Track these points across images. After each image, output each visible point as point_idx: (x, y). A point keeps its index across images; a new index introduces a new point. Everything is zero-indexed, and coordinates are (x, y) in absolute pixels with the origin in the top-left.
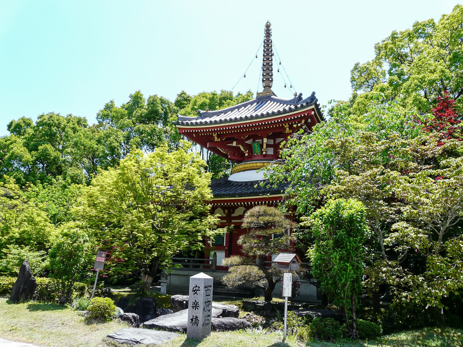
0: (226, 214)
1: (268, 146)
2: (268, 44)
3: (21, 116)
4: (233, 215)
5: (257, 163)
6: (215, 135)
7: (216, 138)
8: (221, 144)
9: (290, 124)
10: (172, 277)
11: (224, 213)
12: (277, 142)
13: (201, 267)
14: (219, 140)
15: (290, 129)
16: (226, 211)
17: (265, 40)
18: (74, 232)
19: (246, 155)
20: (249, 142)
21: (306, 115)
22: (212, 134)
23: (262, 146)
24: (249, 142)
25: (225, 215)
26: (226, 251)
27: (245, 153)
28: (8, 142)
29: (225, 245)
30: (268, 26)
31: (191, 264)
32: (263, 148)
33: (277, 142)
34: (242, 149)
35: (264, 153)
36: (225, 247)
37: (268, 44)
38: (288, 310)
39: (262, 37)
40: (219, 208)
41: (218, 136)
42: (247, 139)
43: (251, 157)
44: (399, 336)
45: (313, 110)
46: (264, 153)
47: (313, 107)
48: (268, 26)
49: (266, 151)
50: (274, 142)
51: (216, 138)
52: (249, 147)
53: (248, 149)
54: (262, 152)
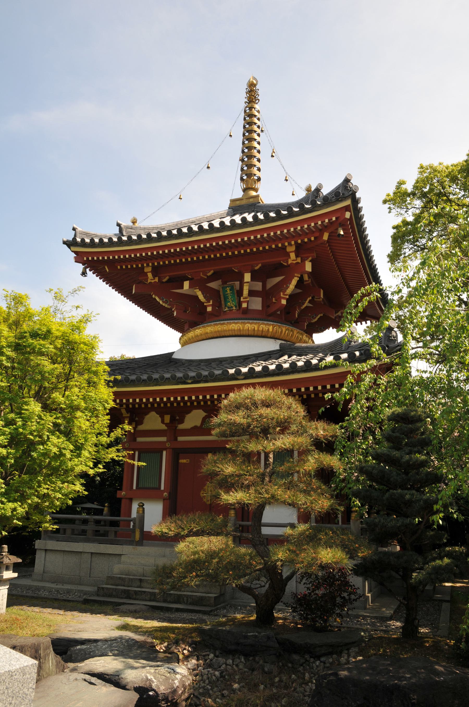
0: (166, 425)
1: (252, 293)
2: (250, 118)
4: (181, 427)
5: (230, 323)
7: (150, 275)
8: (161, 288)
9: (299, 241)
10: (50, 557)
11: (163, 422)
12: (269, 286)
13: (111, 536)
14: (157, 280)
15: (297, 256)
16: (167, 418)
17: (246, 107)
19: (209, 309)
20: (214, 285)
21: (334, 219)
23: (240, 293)
24: (214, 285)
25: (164, 427)
26: (164, 499)
27: (206, 307)
29: (162, 488)
30: (95, 685)
31: (90, 528)
32: (242, 295)
33: (269, 286)
34: (201, 297)
35: (244, 305)
36: (164, 491)
37: (250, 118)
38: (119, 516)
39: (242, 98)
40: (153, 414)
41: (156, 271)
42: (212, 278)
43: (218, 315)
45: (347, 208)
46: (244, 305)
47: (348, 202)
48: (95, 685)
49: (248, 302)
50: (264, 286)
54: (240, 304)
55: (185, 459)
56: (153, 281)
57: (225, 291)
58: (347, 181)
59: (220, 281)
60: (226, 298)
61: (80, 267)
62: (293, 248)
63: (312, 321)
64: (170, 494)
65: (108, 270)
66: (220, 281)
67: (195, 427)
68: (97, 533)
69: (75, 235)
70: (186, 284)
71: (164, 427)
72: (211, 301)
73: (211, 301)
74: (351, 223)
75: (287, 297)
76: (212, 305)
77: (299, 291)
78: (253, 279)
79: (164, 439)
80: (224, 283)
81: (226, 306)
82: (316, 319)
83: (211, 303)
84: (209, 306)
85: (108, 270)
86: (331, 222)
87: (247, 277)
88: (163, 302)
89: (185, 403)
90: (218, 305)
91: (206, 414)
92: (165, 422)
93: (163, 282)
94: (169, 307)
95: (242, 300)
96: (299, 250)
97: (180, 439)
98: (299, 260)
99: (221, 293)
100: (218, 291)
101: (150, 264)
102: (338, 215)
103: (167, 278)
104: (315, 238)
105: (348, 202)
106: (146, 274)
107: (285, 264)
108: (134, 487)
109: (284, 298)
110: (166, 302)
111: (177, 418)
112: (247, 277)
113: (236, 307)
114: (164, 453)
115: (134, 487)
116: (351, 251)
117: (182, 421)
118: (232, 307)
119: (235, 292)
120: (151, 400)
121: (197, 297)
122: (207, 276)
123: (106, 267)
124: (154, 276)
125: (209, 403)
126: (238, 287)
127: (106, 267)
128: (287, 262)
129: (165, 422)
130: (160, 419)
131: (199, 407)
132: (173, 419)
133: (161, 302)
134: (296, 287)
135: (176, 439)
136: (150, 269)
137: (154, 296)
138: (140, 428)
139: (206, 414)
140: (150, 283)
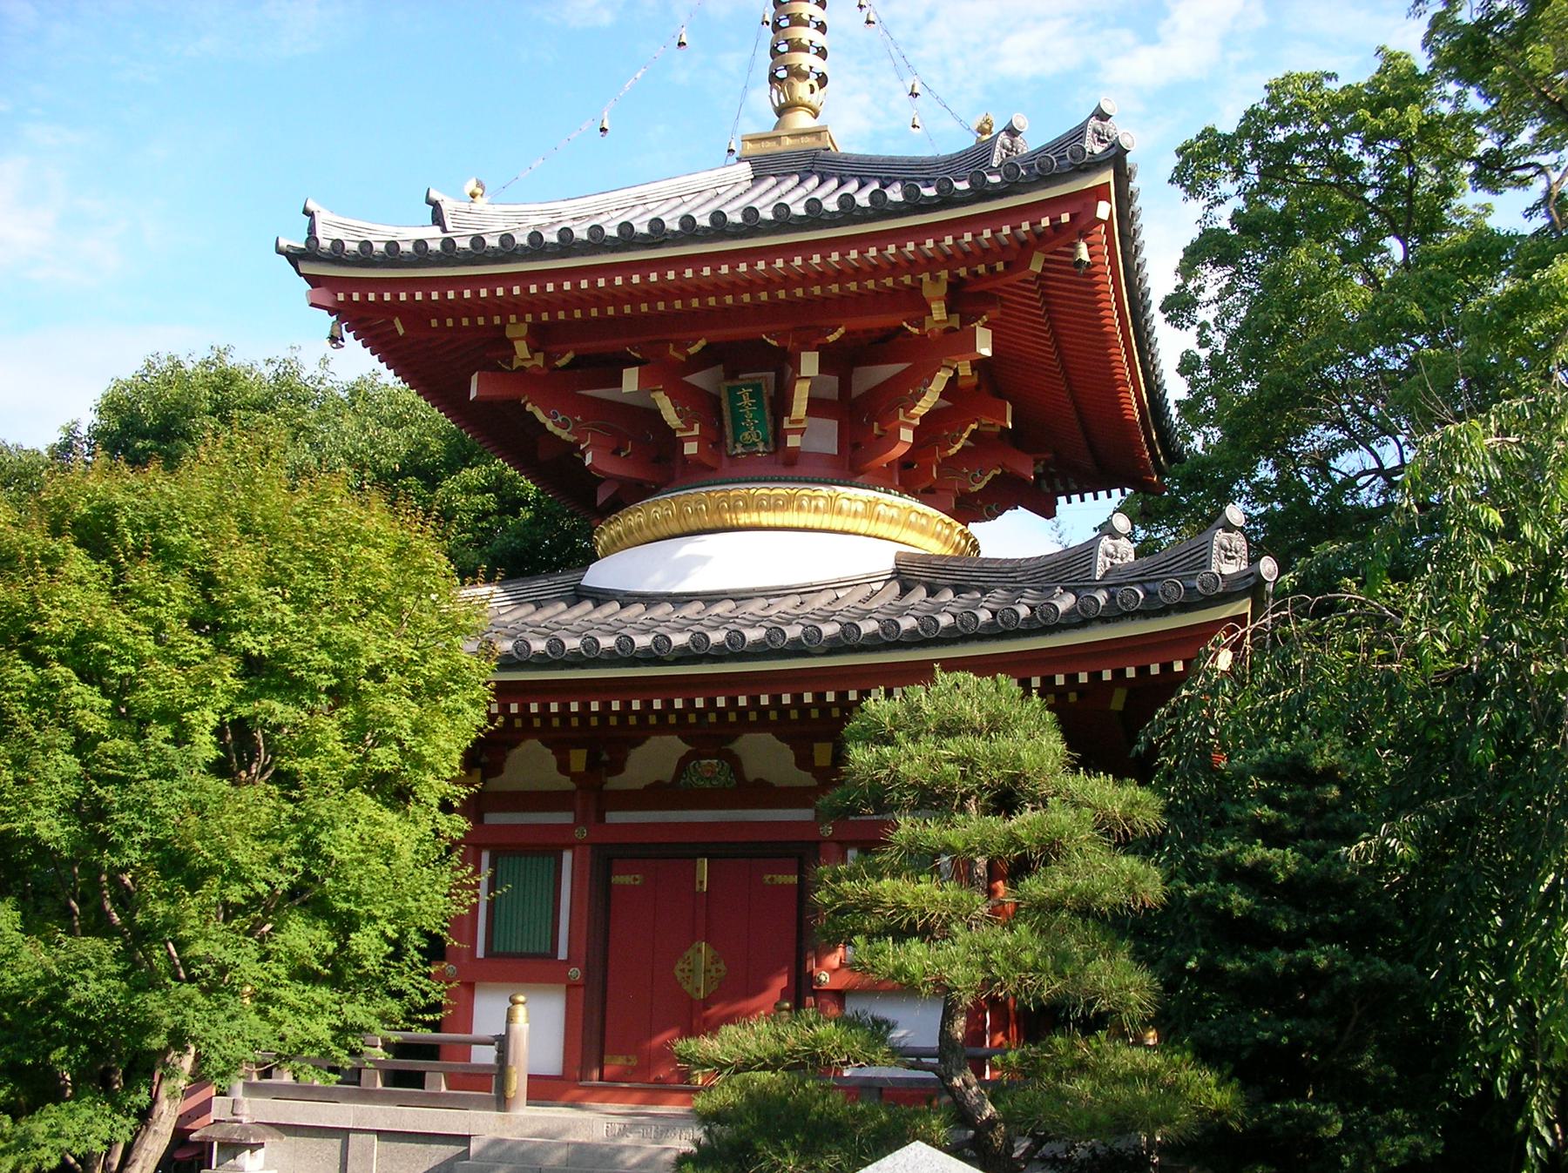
0: (574, 777)
3: (16, 441)
4: (614, 783)
6: (517, 331)
7: (522, 349)
11: (564, 768)
14: (539, 360)
15: (949, 311)
16: (578, 759)
18: (107, 511)
19: (691, 449)
21: (1065, 218)
22: (505, 321)
23: (781, 404)
24: (697, 379)
25: (566, 783)
26: (571, 987)
27: (681, 442)
28: (241, 616)
29: (562, 954)
40: (532, 746)
41: (540, 337)
44: (692, 1042)
50: (845, 386)
51: (522, 349)
52: (706, 409)
53: (699, 420)
54: (779, 436)
55: (629, 873)
56: (528, 365)
57: (735, 399)
58: (1171, 181)
59: (721, 367)
60: (737, 418)
61: (325, 321)
62: (943, 289)
63: (972, 490)
64: (587, 973)
65: (401, 331)
66: (721, 367)
67: (657, 786)
68: (396, 1078)
69: (312, 229)
70: (631, 380)
71: (566, 783)
72: (697, 426)
73: (697, 426)
74: (1109, 232)
75: (917, 422)
76: (700, 439)
77: (946, 403)
78: (823, 367)
79: (566, 818)
80: (731, 374)
81: (736, 441)
82: (981, 486)
83: (696, 432)
84: (691, 439)
85: (401, 331)
86: (1056, 226)
87: (810, 363)
88: (556, 424)
89: (804, 710)
90: (714, 439)
91: (731, 747)
92: (573, 769)
93: (557, 368)
94: (572, 438)
95: (786, 425)
96: (957, 297)
97: (613, 817)
98: (955, 322)
99: (725, 405)
100: (718, 399)
101: (529, 318)
102: (1077, 207)
103: (570, 356)
104: (1007, 265)
105: (1108, 176)
106: (509, 345)
107: (916, 331)
108: (480, 953)
109: (908, 425)
110: (564, 426)
111: (605, 757)
112: (810, 363)
113: (766, 444)
114: (567, 857)
115: (480, 953)
116: (1087, 293)
117: (617, 767)
118: (755, 444)
119: (766, 401)
120: (657, 704)
121: (657, 413)
122: (688, 356)
123: (397, 321)
124: (533, 350)
125: (556, 722)
126: (769, 387)
127: (397, 321)
128: (921, 325)
129: (573, 769)
130: (552, 761)
131: (663, 727)
132: (593, 763)
133: (550, 426)
134: (943, 395)
135: (602, 819)
136: (523, 330)
137: (529, 407)
138: (496, 784)
139: (731, 747)
140: (522, 368)
